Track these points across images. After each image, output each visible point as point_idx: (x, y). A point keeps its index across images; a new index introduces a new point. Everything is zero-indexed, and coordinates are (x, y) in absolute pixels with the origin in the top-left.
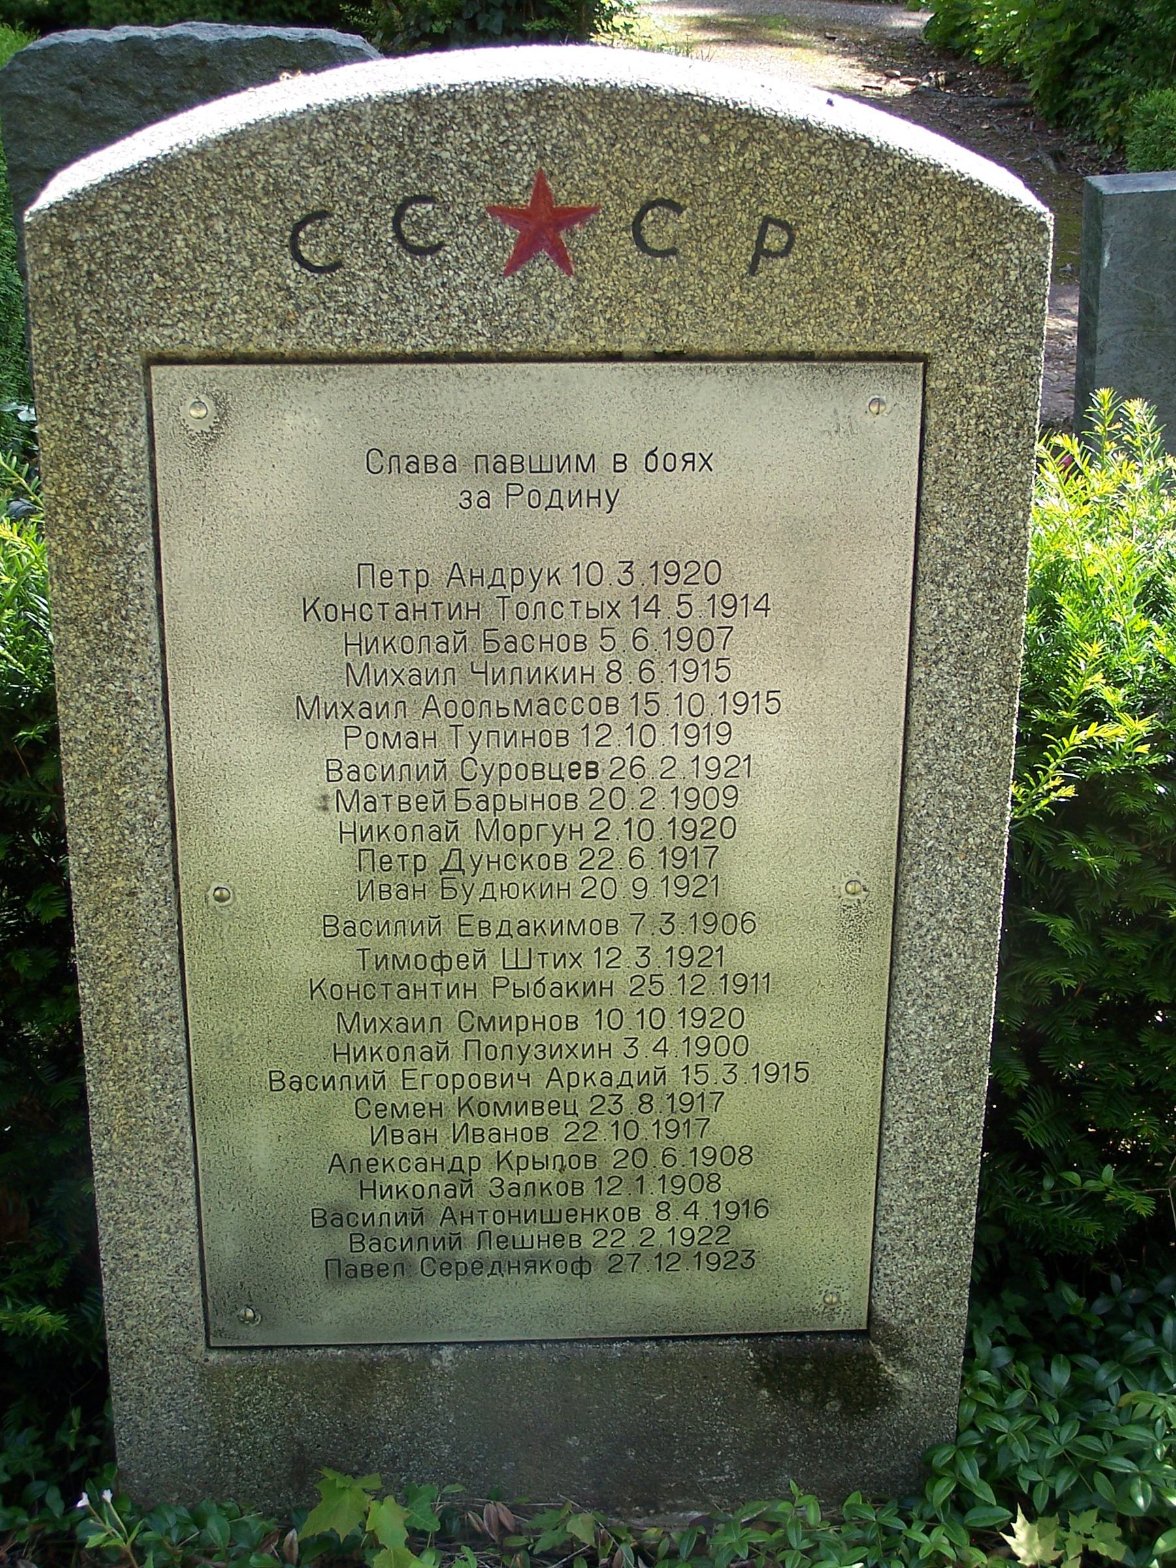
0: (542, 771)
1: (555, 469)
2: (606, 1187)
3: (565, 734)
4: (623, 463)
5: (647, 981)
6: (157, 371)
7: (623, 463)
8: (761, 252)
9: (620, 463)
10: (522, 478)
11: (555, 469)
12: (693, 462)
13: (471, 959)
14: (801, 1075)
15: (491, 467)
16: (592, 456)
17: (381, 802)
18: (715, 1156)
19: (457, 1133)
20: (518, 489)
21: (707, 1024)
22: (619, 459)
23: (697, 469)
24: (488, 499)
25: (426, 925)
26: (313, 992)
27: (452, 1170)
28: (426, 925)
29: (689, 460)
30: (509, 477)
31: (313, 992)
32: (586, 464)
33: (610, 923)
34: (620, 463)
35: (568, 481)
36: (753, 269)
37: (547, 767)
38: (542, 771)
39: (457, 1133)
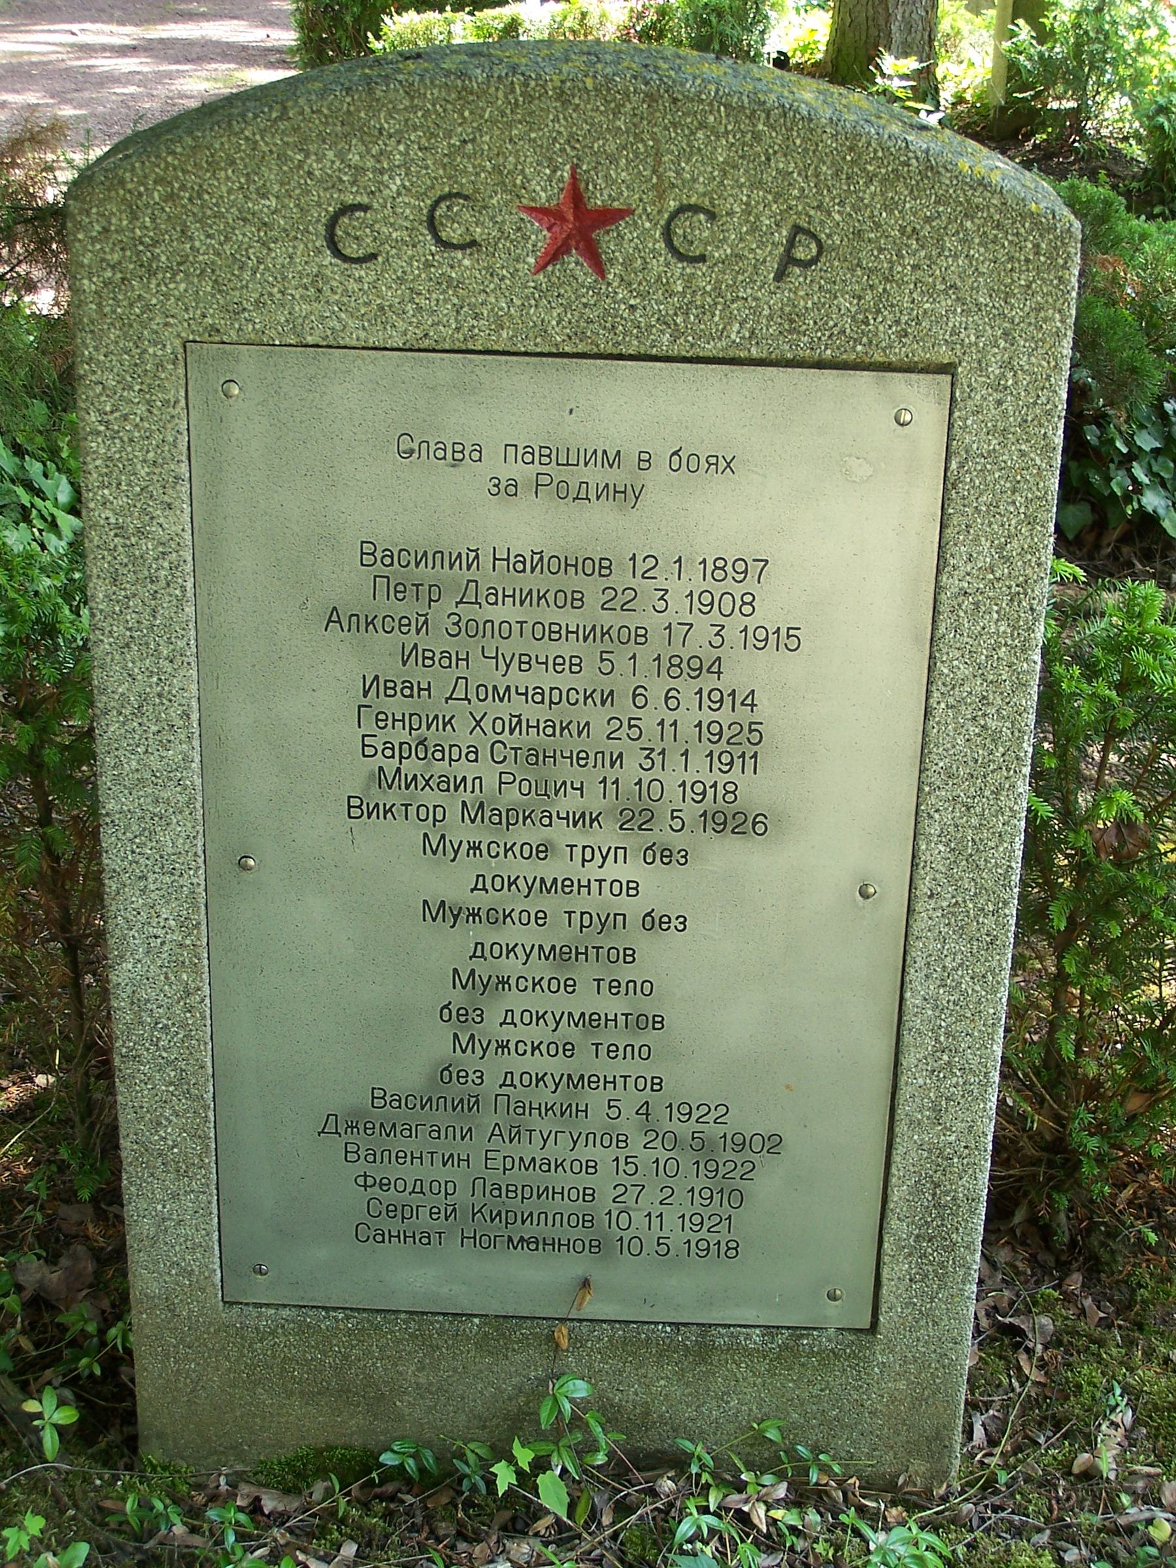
0: (559, 632)
1: (582, 462)
2: (641, 568)
3: (578, 661)
4: (648, 461)
5: (626, 724)
6: (949, 378)
7: (648, 461)
8: (789, 259)
9: (645, 461)
10: (552, 469)
11: (582, 462)
12: (717, 464)
13: (443, 1212)
14: (793, 643)
15: (519, 458)
16: (619, 452)
17: (411, 590)
18: (712, 604)
19: (406, 653)
20: (547, 480)
21: (705, 1228)
22: (643, 456)
23: (720, 471)
24: (516, 487)
25: (466, 1102)
26: (474, 1215)
27: (413, 1192)
28: (466, 1102)
29: (712, 462)
30: (537, 468)
31: (474, 1215)
32: (613, 460)
33: (588, 1192)
34: (645, 461)
35: (596, 475)
36: (780, 275)
37: (554, 452)
38: (549, 456)
39: (406, 653)
